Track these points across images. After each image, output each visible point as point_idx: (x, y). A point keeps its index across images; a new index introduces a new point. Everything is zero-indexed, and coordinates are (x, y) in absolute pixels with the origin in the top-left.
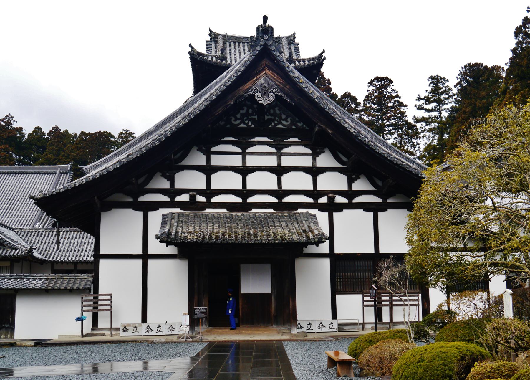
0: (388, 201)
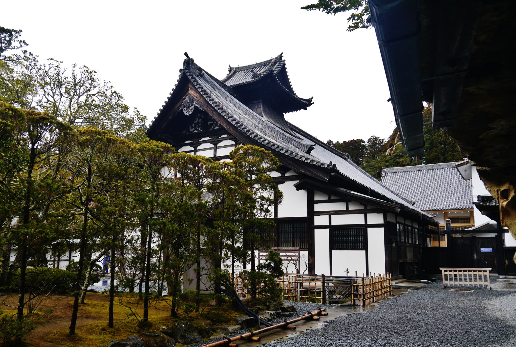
0: (286, 175)
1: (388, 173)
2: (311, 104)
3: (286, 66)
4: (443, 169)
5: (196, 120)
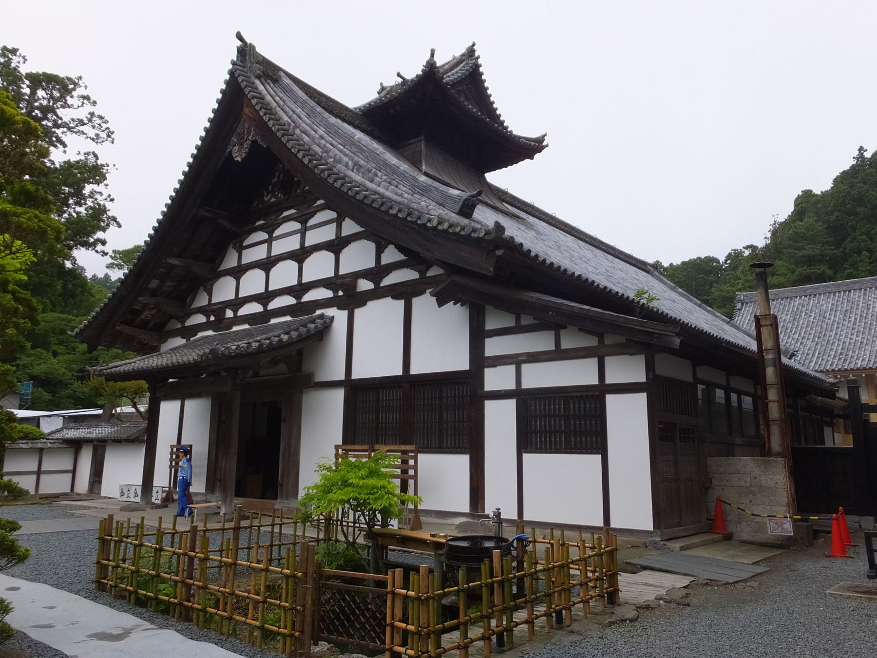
0: (429, 274)
1: (747, 303)
2: (543, 148)
3: (481, 69)
4: (860, 290)
5: (274, 177)
